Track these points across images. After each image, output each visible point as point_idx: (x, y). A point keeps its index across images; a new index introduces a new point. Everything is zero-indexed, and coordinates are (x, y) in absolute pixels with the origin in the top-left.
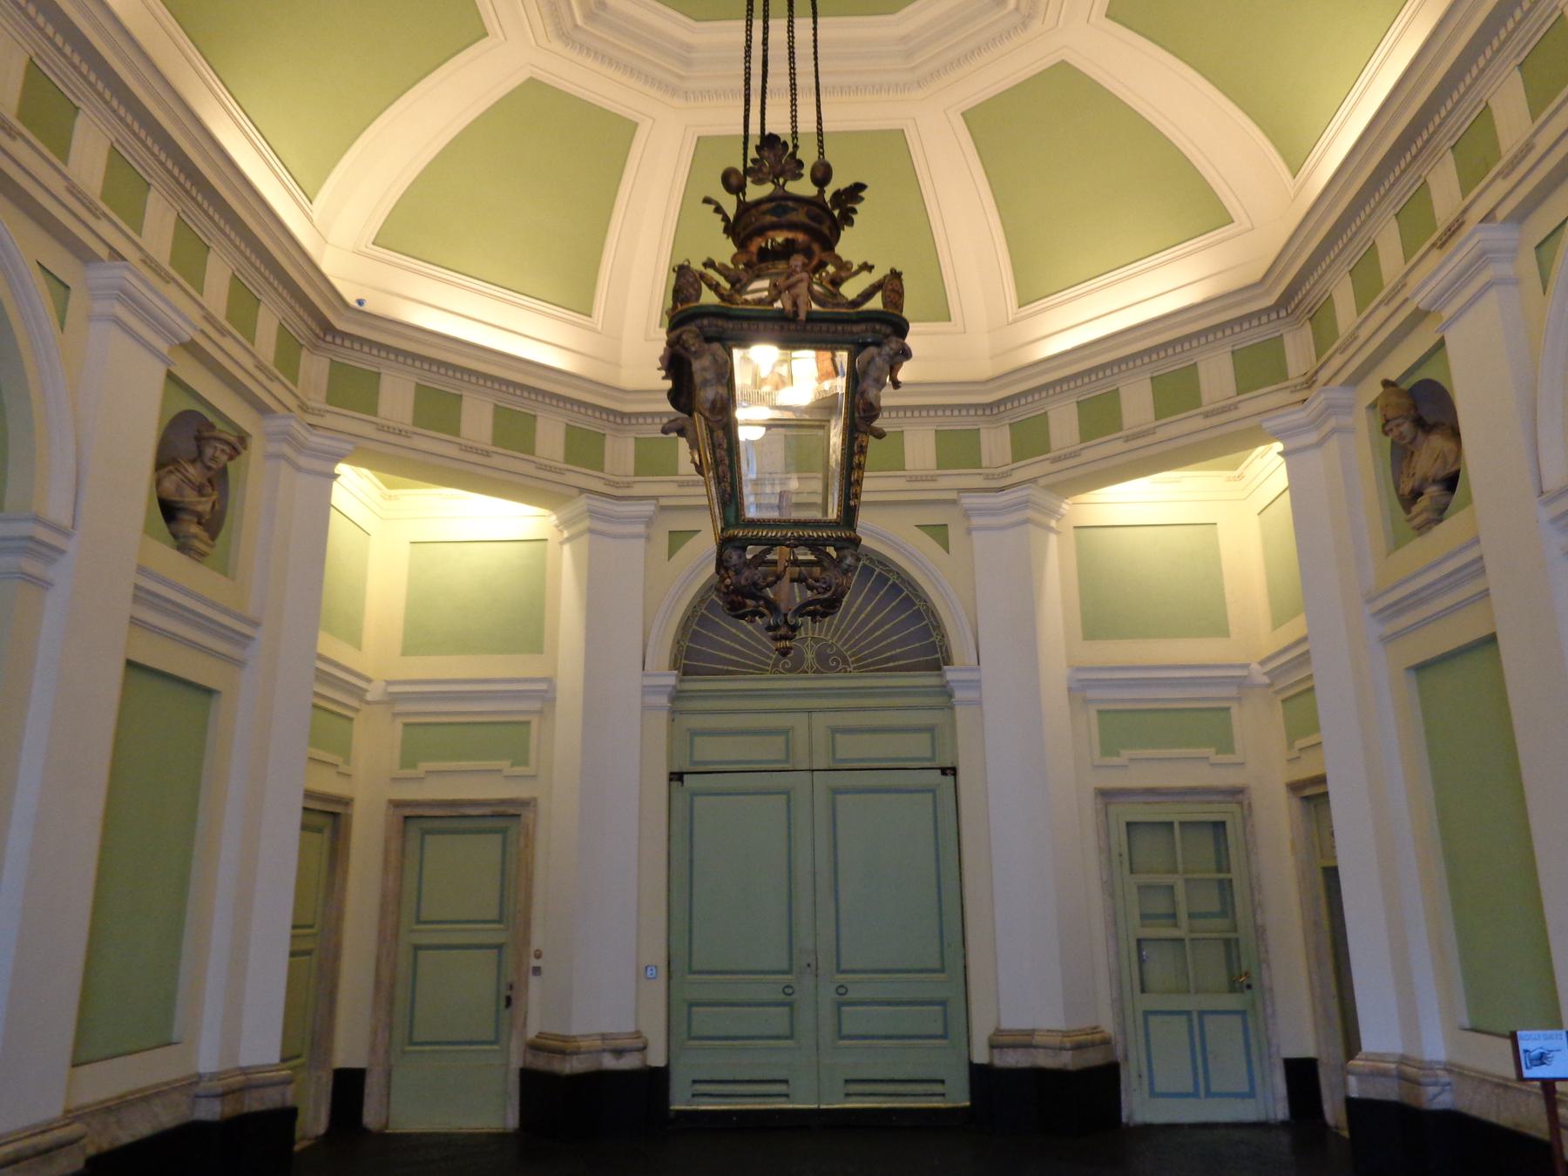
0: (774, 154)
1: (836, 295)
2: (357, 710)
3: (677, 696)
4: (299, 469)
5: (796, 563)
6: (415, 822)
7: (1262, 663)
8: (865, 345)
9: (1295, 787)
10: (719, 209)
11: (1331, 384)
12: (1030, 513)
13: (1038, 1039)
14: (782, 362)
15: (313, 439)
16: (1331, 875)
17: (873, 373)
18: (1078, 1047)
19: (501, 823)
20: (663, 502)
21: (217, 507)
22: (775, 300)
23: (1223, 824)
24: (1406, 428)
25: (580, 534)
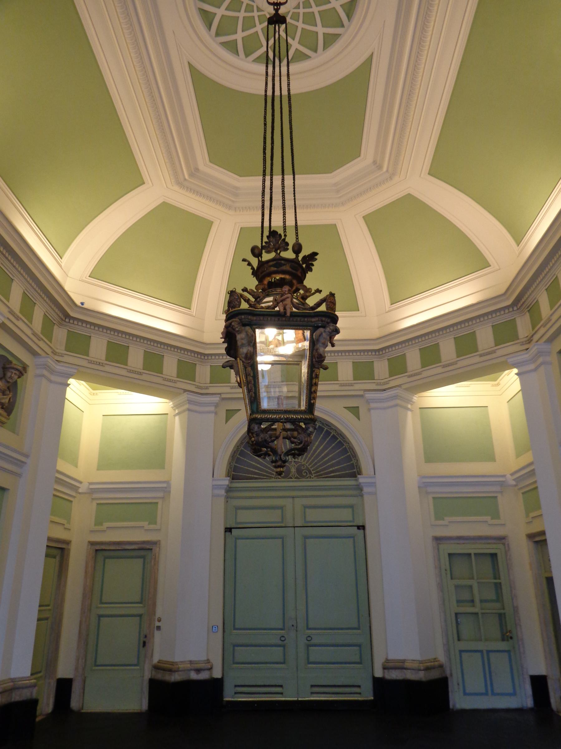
0: (275, 239)
1: (304, 304)
2: (74, 497)
3: (229, 490)
4: (50, 381)
5: (285, 430)
6: (101, 552)
7: (512, 474)
8: (318, 327)
9: (530, 536)
10: (249, 264)
11: (539, 343)
12: (398, 402)
13: (407, 665)
14: (279, 334)
15: (58, 367)
16: (550, 581)
17: (322, 340)
18: (427, 669)
19: (142, 553)
20: (223, 396)
21: (11, 400)
22: (276, 307)
23: (496, 555)
25: (184, 411)
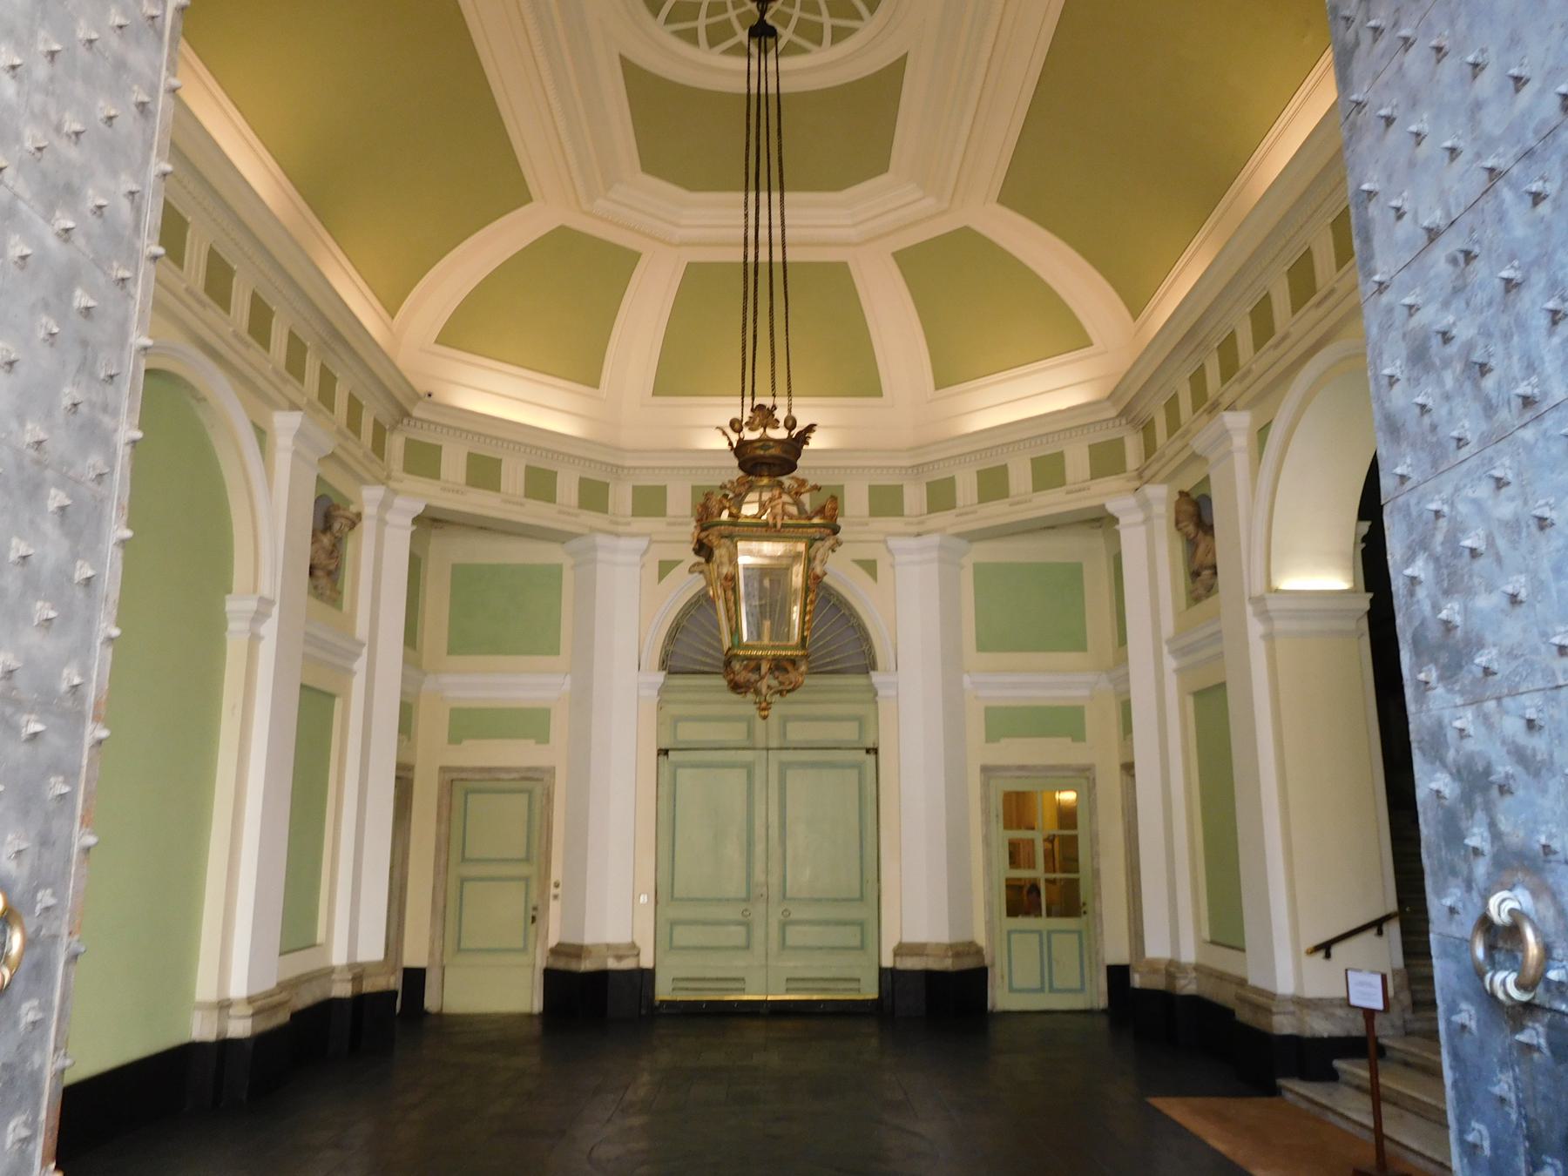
3: (664, 690)
20: (655, 538)
24: (1191, 529)
